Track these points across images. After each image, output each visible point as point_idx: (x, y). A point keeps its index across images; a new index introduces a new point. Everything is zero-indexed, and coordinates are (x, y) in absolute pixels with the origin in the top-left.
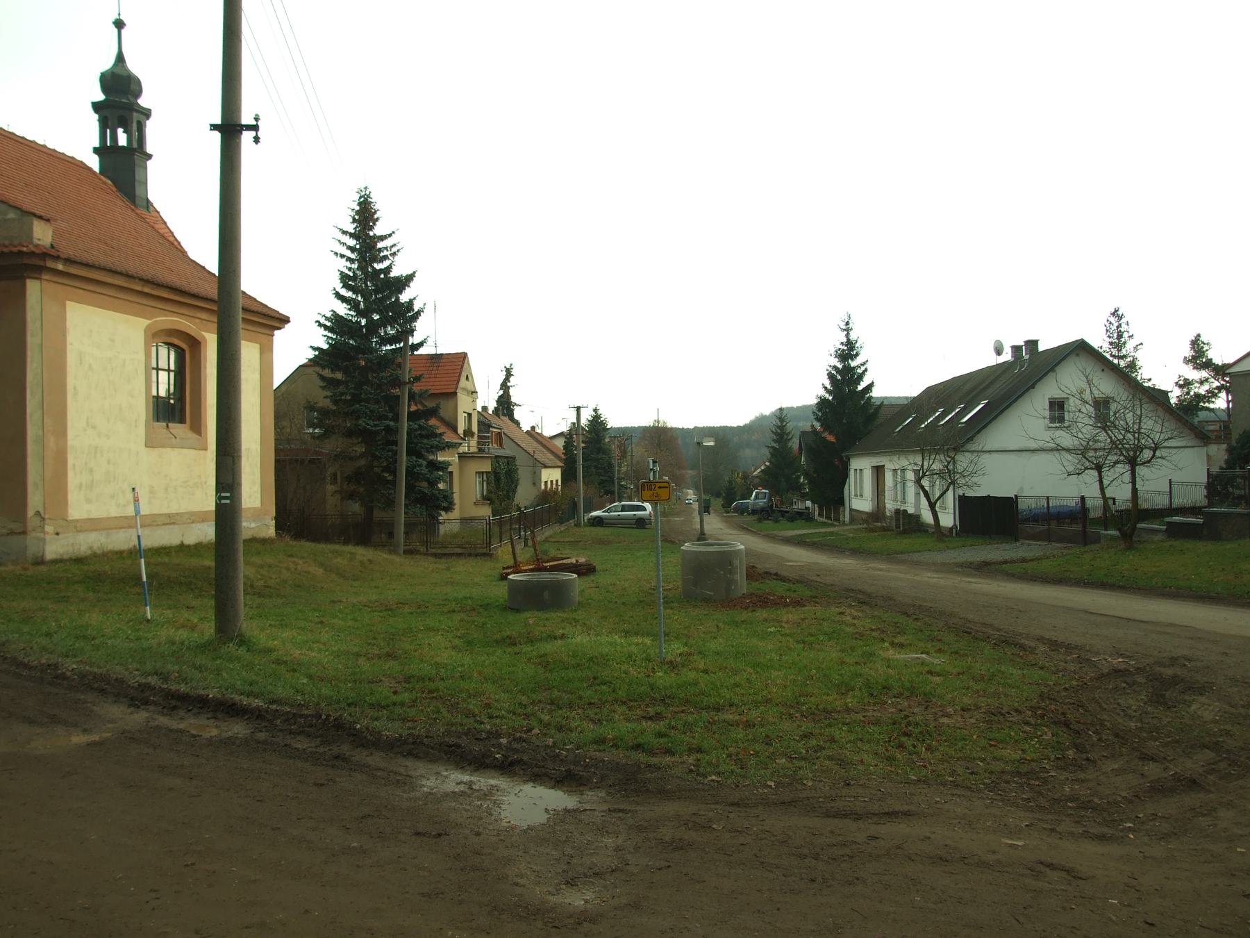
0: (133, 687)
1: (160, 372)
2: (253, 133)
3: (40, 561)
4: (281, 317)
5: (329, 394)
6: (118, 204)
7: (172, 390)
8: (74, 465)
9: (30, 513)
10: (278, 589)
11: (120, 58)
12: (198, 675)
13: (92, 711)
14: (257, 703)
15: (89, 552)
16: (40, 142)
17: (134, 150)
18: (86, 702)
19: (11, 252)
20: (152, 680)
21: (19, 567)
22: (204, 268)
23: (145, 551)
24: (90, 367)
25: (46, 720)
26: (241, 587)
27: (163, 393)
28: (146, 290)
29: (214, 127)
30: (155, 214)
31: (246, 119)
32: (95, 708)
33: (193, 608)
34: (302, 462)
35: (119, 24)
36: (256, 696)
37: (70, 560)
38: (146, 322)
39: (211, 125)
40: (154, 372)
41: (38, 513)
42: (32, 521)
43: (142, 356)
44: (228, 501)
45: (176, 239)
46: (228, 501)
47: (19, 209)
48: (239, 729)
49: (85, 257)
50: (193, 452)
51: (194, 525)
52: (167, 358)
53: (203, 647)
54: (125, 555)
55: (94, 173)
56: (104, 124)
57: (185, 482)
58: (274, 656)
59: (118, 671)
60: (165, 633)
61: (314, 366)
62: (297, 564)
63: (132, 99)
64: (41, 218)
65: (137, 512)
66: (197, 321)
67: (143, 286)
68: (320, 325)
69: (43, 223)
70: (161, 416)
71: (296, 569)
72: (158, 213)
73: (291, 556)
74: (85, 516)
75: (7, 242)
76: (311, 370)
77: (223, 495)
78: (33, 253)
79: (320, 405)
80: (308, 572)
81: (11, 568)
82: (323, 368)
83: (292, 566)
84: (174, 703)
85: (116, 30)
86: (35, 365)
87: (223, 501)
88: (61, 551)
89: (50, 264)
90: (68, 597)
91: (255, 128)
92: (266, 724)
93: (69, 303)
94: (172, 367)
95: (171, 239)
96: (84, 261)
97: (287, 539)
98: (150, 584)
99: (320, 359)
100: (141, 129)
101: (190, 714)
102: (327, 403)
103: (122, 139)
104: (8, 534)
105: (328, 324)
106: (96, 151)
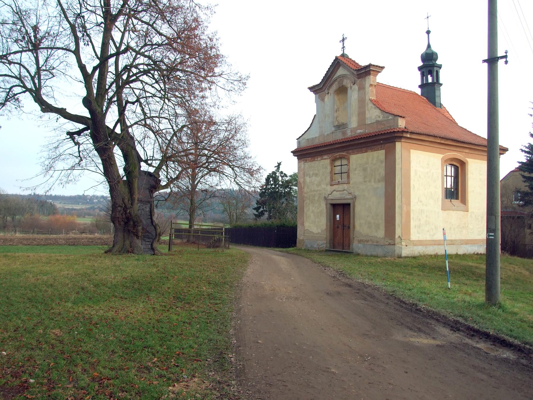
0: (451, 321)
1: (448, 177)
2: (504, 60)
3: (400, 257)
4: (504, 148)
5: (527, 184)
6: (429, 107)
7: (452, 186)
8: (413, 218)
9: (397, 237)
10: (507, 280)
11: (429, 46)
12: (481, 321)
13: (435, 329)
14: (517, 342)
15: (418, 255)
16: (399, 87)
17: (435, 83)
18: (431, 324)
19: (388, 133)
20: (460, 320)
21: (393, 258)
22: (466, 130)
23: (448, 255)
24: (420, 177)
25: (416, 329)
26: (499, 280)
27: (449, 187)
28: (442, 142)
29: (484, 61)
30: (444, 109)
31: (500, 53)
32: (436, 328)
33: (466, 284)
34: (514, 218)
35: (428, 32)
36: (515, 338)
37: (411, 257)
38: (442, 156)
39: (483, 60)
40: (445, 177)
41: (399, 237)
42: (397, 240)
43: (440, 171)
44: (493, 237)
45: (453, 119)
46: (493, 237)
47: (393, 114)
48: (508, 354)
49: (418, 131)
50: (462, 213)
51: (462, 245)
52: (450, 171)
53: (480, 306)
54: (433, 256)
55: (419, 96)
56: (423, 75)
57: (458, 226)
58: (518, 317)
59: (443, 312)
60: (460, 296)
61: (519, 171)
62: (515, 268)
63: (434, 62)
64: (401, 117)
65: (444, 237)
66: (464, 153)
67: (441, 140)
68: (522, 151)
69: (402, 119)
70: (448, 196)
71: (514, 271)
72: (445, 108)
73: (510, 264)
74: (417, 239)
75: (389, 128)
76: (517, 173)
77: (490, 234)
78: (398, 131)
79: (522, 190)
80: (521, 273)
81: (390, 258)
82: (524, 172)
83: (512, 269)
84: (472, 333)
85: (427, 35)
86: (399, 176)
87: (490, 237)
88: (408, 253)
89: (405, 135)
90: (412, 273)
91: (505, 57)
92: (525, 355)
93: (411, 150)
94: (453, 175)
95: (451, 119)
96: (418, 132)
97: (507, 255)
98: (450, 272)
99: (523, 167)
100: (437, 73)
101: (481, 340)
102: (527, 189)
103: (430, 80)
104: (388, 245)
105: (527, 150)
106: (420, 86)
